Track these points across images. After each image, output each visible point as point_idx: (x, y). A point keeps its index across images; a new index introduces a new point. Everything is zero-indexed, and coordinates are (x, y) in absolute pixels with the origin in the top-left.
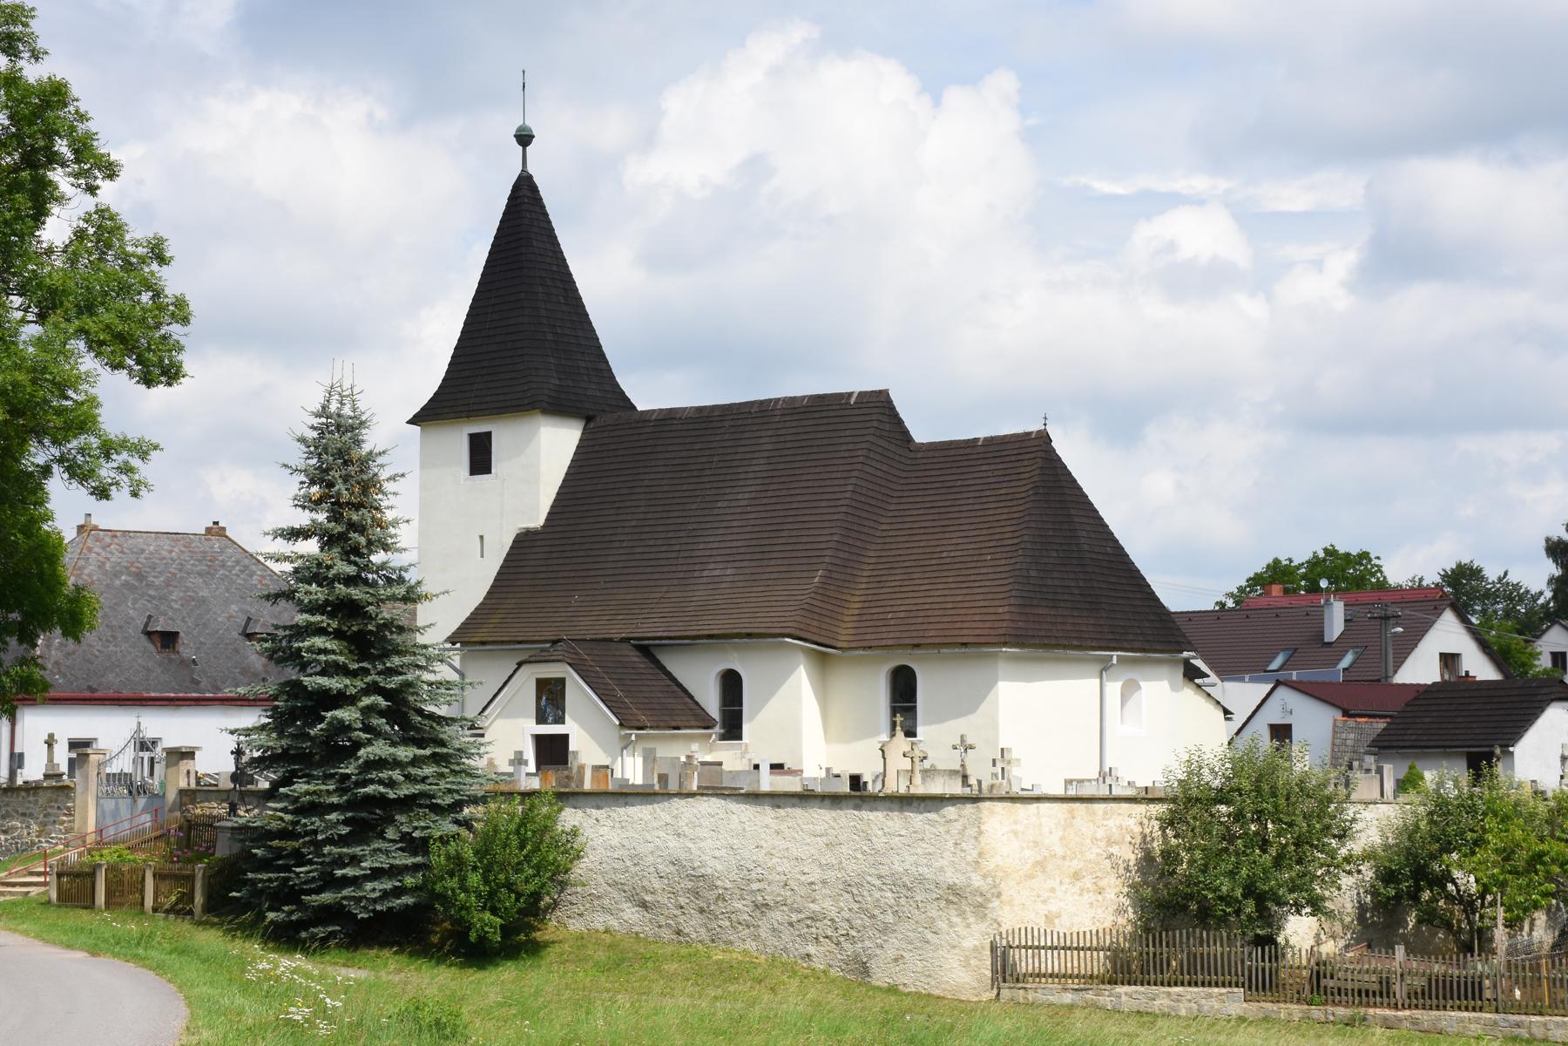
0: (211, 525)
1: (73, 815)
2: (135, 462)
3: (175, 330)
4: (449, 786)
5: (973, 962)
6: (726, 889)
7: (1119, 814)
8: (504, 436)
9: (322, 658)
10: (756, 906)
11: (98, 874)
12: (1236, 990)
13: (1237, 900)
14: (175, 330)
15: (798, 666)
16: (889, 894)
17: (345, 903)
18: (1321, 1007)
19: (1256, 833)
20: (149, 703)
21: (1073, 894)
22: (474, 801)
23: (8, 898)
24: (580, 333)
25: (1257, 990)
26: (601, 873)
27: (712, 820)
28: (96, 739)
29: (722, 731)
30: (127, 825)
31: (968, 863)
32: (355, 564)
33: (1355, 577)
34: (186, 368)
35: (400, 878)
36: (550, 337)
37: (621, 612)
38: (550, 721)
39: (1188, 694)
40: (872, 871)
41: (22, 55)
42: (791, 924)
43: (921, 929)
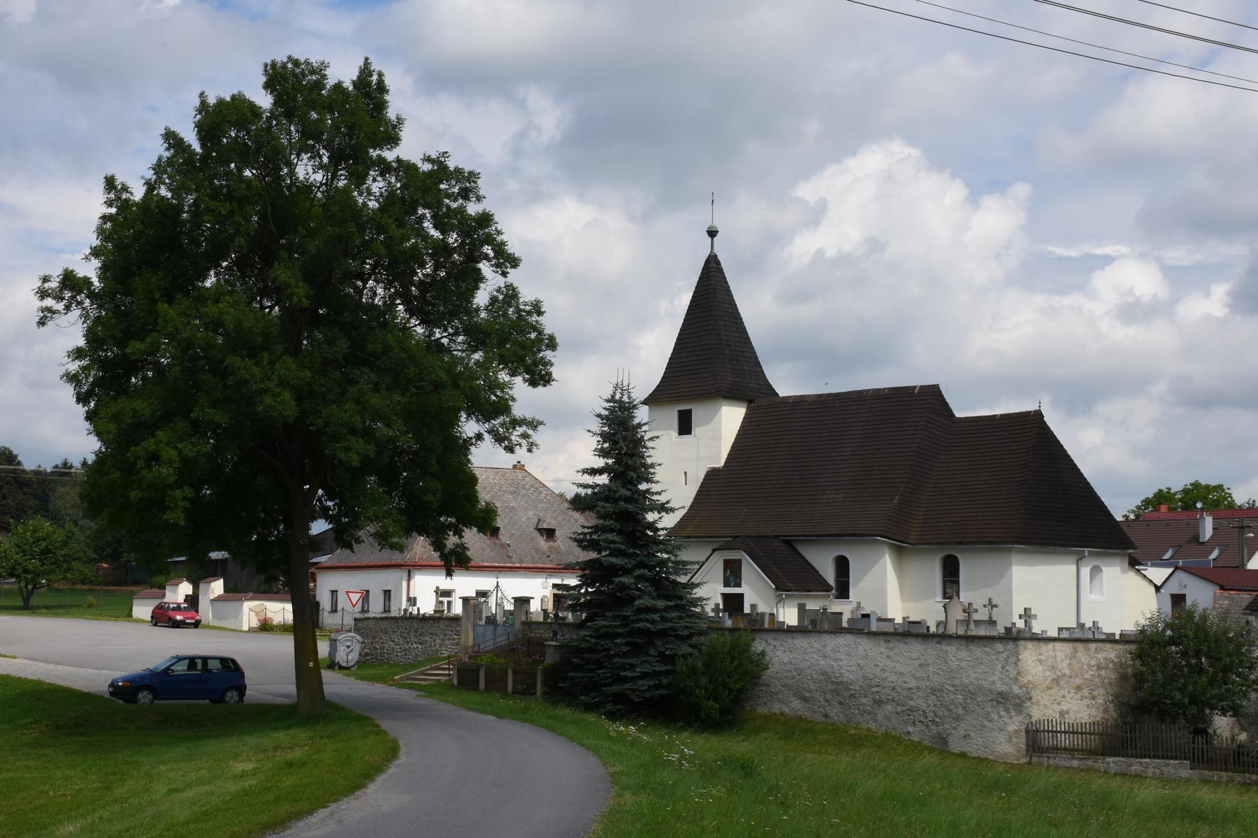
0: (516, 463)
1: (460, 635)
2: (530, 432)
3: (548, 354)
4: (686, 624)
5: (1014, 740)
6: (856, 690)
7: (1105, 651)
8: (698, 412)
9: (612, 546)
10: (875, 701)
11: (481, 670)
12: (1184, 762)
13: (1185, 706)
14: (548, 354)
15: (884, 555)
16: (960, 697)
17: (627, 692)
18: (1242, 774)
19: (1196, 664)
20: (484, 569)
21: (1076, 700)
22: (700, 633)
23: (428, 682)
24: (745, 350)
25: (1198, 762)
26: (778, 679)
27: (847, 648)
28: (454, 590)
29: (837, 593)
30: (491, 642)
31: (1011, 679)
32: (630, 490)
33: (1214, 501)
34: (554, 376)
35: (658, 678)
36: (727, 352)
37: (772, 519)
38: (732, 584)
39: (1131, 576)
40: (949, 682)
41: (472, 199)
42: (897, 713)
43: (981, 719)
